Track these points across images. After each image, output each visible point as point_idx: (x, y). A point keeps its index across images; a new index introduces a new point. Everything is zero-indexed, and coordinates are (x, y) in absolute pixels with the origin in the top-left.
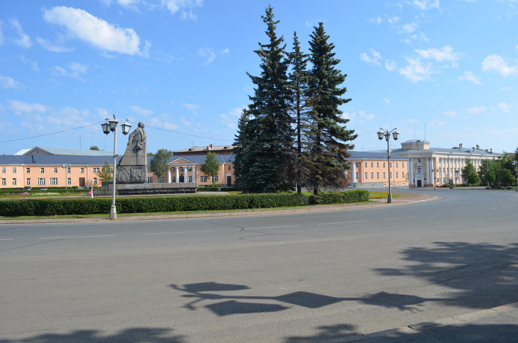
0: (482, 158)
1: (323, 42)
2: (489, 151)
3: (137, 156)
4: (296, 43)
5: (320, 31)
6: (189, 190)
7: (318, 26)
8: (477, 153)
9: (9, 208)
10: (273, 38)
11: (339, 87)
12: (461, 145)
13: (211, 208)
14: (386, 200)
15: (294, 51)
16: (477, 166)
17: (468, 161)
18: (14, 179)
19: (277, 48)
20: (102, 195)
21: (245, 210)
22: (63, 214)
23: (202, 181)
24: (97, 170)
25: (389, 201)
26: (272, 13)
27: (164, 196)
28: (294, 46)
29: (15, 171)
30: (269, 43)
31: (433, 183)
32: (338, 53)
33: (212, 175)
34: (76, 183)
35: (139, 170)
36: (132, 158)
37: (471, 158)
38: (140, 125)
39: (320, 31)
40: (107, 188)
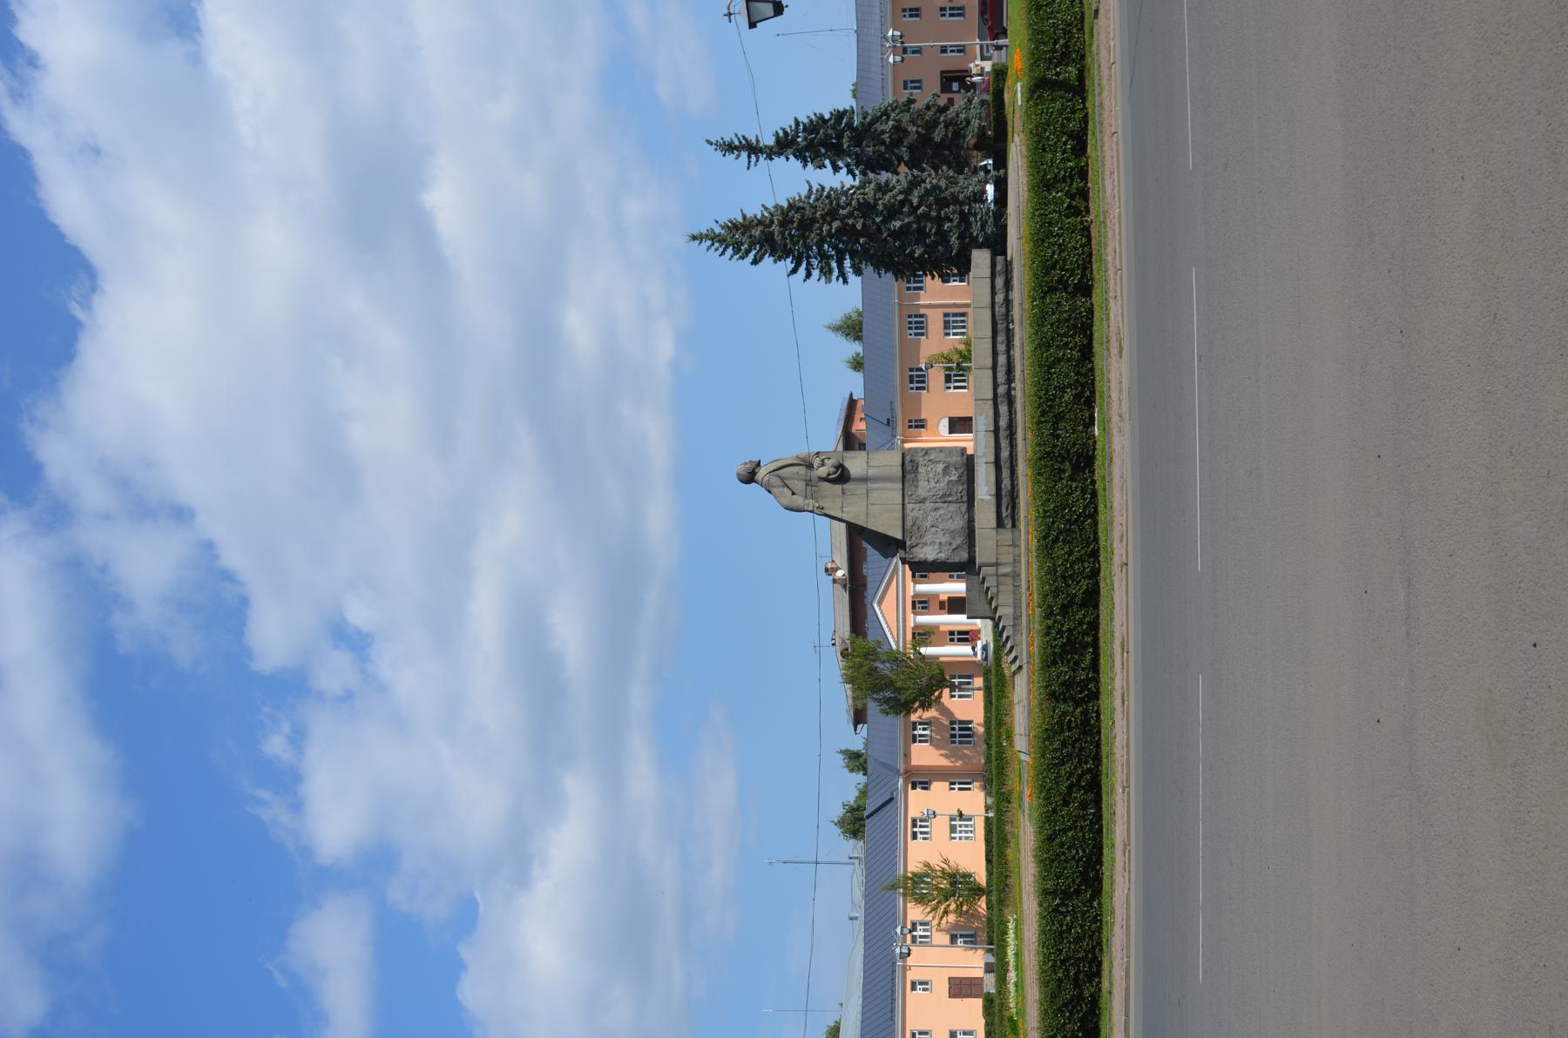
6: (1000, 281)
20: (1016, 587)
27: (1022, 390)
36: (874, 495)
38: (749, 477)
40: (992, 570)
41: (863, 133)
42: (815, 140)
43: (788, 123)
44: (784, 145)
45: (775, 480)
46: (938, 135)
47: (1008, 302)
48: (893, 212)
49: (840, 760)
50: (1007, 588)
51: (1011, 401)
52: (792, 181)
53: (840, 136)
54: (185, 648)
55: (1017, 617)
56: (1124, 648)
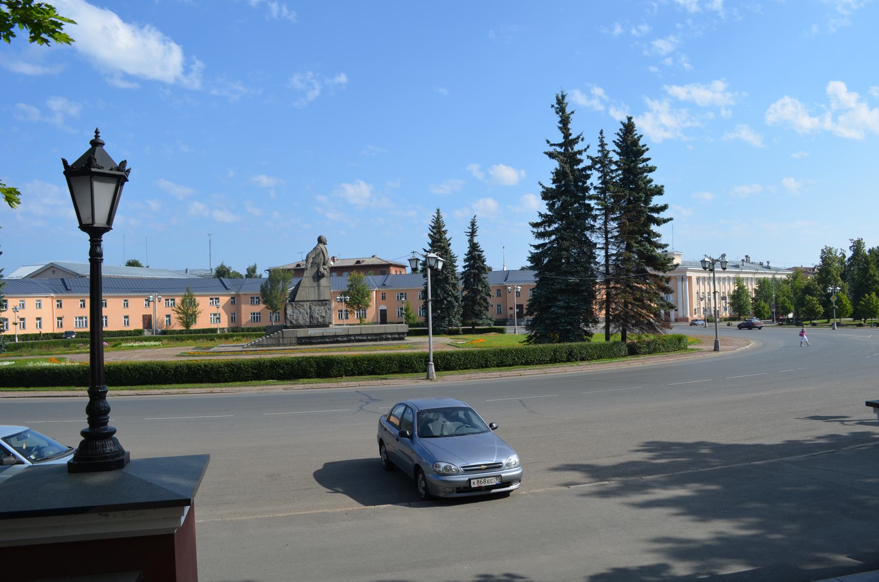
0: (757, 276)
1: (635, 143)
2: (765, 264)
3: (319, 286)
4: (602, 145)
5: (629, 128)
6: (397, 336)
7: (626, 122)
8: (750, 268)
9: (283, 368)
10: (567, 135)
11: (656, 201)
12: (724, 256)
13: (501, 364)
14: (713, 348)
15: (600, 155)
16: (751, 288)
17: (738, 281)
18: (39, 319)
19: (572, 149)
20: (274, 345)
21: (544, 366)
22: (353, 375)
23: (340, 317)
24: (170, 302)
25: (716, 349)
26: (566, 101)
28: (600, 148)
29: (39, 306)
30: (561, 140)
31: (688, 316)
32: (653, 157)
33: (359, 309)
34: (137, 324)
35: (322, 308)
36: (312, 289)
37: (741, 276)
38: (320, 240)
39: (629, 128)
41: (478, 278)
43: (482, 248)
44: (474, 247)
46: (477, 308)
49: (252, 265)
50: (274, 342)
52: (459, 249)
53: (477, 268)
54: (194, 57)
56: (469, 378)
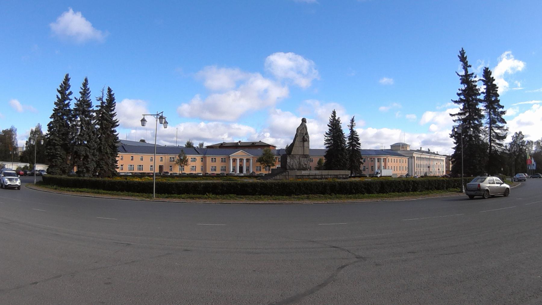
6: (344, 176)
42: (354, 137)
44: (353, 132)
45: (303, 126)
47: (340, 178)
48: (342, 155)
51: (321, 179)
52: (346, 132)
55: (277, 179)
